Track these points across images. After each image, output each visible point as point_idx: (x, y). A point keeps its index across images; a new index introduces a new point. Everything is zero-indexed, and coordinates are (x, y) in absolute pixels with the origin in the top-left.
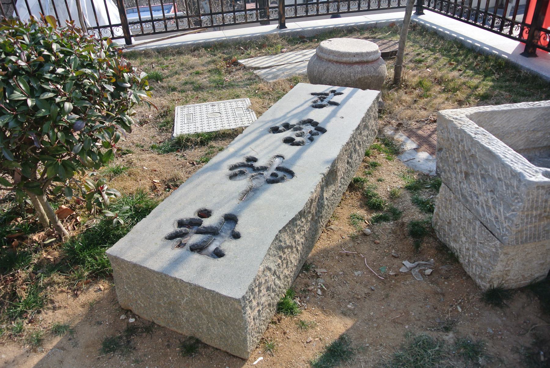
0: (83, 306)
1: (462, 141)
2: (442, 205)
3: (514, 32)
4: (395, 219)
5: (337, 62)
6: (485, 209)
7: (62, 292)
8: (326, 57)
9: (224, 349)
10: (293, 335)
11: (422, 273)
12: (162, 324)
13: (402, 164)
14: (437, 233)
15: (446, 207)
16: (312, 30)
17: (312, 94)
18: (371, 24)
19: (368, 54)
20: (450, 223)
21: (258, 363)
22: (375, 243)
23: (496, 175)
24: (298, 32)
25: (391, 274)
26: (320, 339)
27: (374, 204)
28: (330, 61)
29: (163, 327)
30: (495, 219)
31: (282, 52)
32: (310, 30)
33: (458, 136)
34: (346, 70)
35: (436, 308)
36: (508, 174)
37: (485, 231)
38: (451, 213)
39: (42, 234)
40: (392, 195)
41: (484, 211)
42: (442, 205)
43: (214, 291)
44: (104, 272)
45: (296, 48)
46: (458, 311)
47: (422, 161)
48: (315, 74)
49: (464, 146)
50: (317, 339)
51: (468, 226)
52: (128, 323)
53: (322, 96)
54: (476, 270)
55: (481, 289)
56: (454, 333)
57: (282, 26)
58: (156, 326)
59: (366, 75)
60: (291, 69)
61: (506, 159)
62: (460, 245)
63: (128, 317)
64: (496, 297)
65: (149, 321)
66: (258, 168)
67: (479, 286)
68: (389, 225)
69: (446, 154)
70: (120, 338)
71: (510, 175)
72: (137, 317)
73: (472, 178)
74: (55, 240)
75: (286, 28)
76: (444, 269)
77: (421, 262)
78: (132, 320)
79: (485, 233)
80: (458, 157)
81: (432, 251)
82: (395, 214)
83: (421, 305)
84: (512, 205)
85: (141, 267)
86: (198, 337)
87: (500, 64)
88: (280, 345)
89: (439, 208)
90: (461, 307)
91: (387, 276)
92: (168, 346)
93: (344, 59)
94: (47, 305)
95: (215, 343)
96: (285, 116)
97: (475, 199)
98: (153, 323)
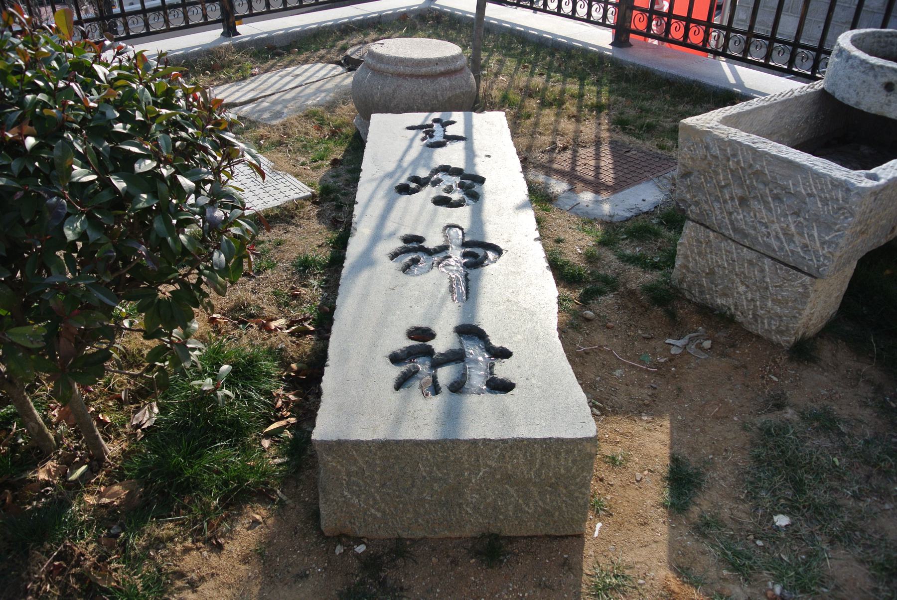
0: (245, 560)
1: (734, 155)
2: (692, 252)
3: (594, 13)
4: (614, 289)
5: (412, 76)
6: (784, 240)
7: (187, 550)
8: (391, 69)
9: (544, 533)
10: (612, 478)
11: (699, 347)
12: (419, 534)
13: (567, 214)
14: (686, 293)
15: (700, 254)
16: (318, 28)
17: (409, 128)
18: (373, 18)
19: (439, 61)
20: (712, 273)
21: (600, 532)
22: (608, 328)
23: (803, 191)
24: (263, 39)
25: (662, 361)
26: (650, 471)
27: (573, 276)
28: (399, 75)
29: (422, 539)
30: (802, 248)
31: (253, 75)
32: (281, 35)
33: (726, 150)
34: (428, 87)
35: (748, 386)
36: (827, 185)
37: (781, 269)
38: (712, 259)
39: (51, 465)
40: (589, 257)
41: (782, 243)
42: (692, 252)
43: (550, 438)
44: (243, 491)
45: (272, 66)
46: (775, 382)
47: (591, 205)
48: (376, 99)
49: (738, 162)
50: (646, 472)
51: (748, 268)
52: (358, 556)
53: (427, 130)
54: (769, 324)
55: (782, 347)
56: (791, 407)
57: (230, 31)
58: (408, 543)
59: (458, 91)
60: (294, 99)
61: (815, 168)
62: (738, 298)
63: (349, 548)
64: (803, 351)
65: (390, 539)
66: (435, 249)
67: (779, 344)
68: (609, 299)
69: (700, 179)
70: (362, 583)
71: (830, 186)
72: (365, 541)
73: (754, 204)
74: (87, 469)
75: (238, 34)
76: (722, 335)
77: (692, 335)
78: (361, 549)
79: (782, 271)
80: (726, 178)
81: (695, 318)
82: (610, 284)
83: (728, 387)
84: (836, 224)
85: (397, 442)
86: (495, 531)
87: (592, 61)
88: (609, 497)
89: (686, 257)
90: (775, 375)
91: (658, 366)
92: (455, 562)
93: (424, 70)
94: (172, 584)
95: (532, 528)
96: (399, 166)
97: (764, 229)
98: (399, 539)
